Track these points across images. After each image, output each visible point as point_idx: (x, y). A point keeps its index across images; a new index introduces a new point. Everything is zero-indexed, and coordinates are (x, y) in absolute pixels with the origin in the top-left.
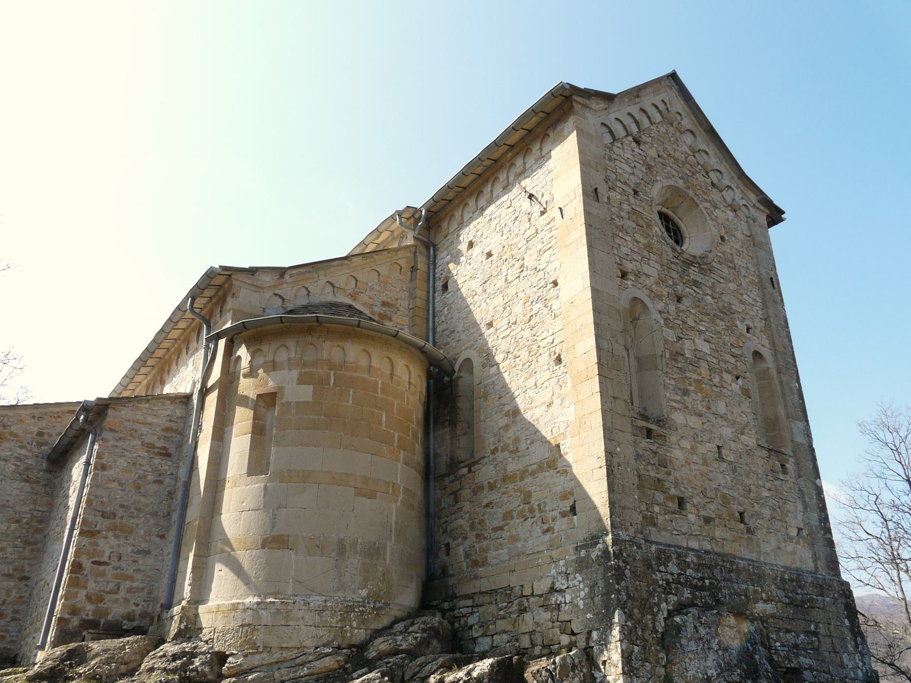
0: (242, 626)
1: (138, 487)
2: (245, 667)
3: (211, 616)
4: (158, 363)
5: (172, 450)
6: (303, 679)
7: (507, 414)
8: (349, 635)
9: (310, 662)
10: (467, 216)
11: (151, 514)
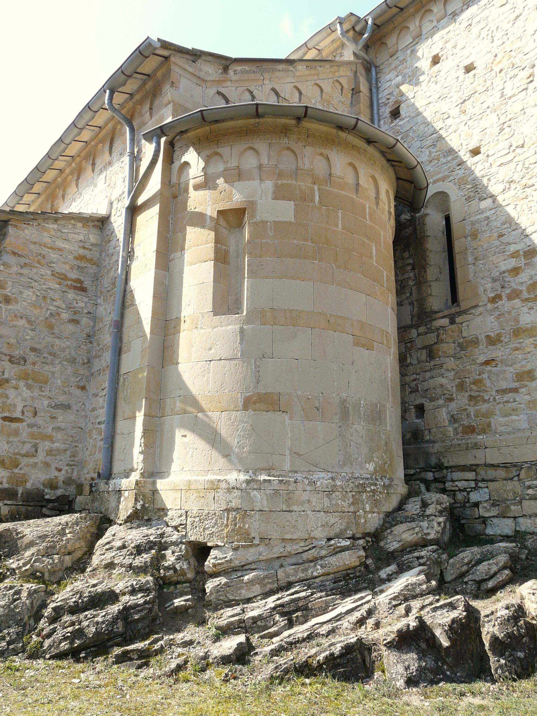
0: (228, 510)
1: (51, 327)
2: (237, 563)
3: (178, 494)
4: (46, 189)
5: (87, 284)
6: (317, 580)
7: (515, 255)
8: (363, 521)
9: (322, 558)
10: (427, 27)
11: (68, 361)
